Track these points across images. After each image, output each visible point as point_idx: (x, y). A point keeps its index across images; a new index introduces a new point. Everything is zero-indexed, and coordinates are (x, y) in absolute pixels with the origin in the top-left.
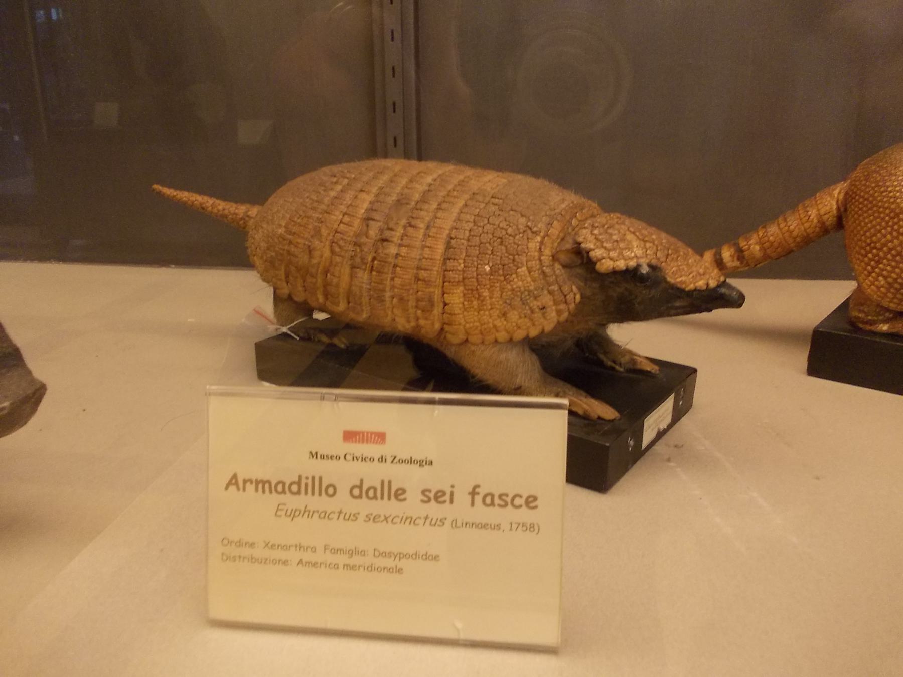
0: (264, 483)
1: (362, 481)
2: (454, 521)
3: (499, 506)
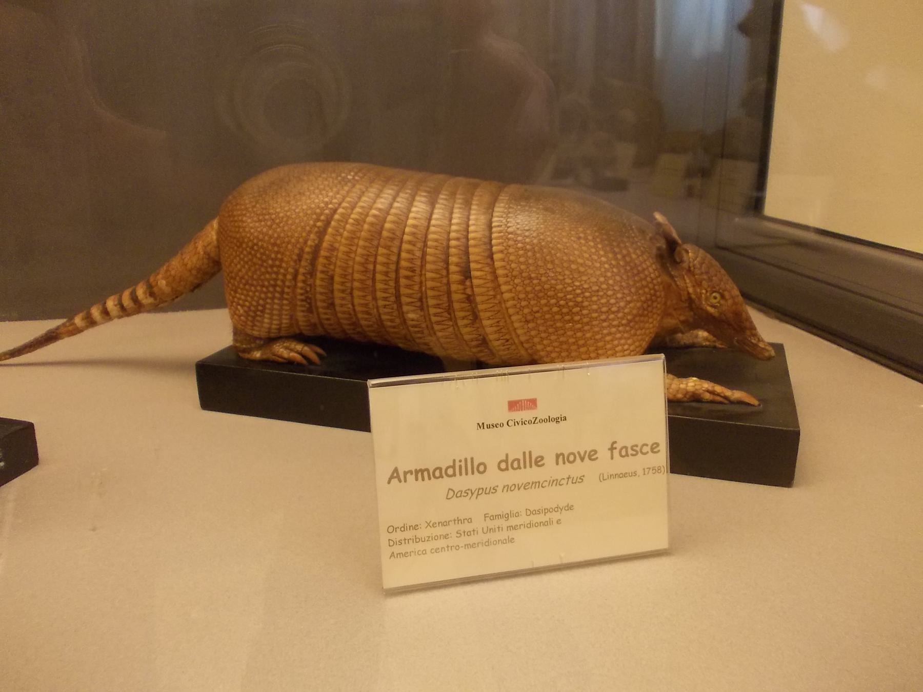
0: (422, 471)
2: (602, 475)
3: (633, 455)
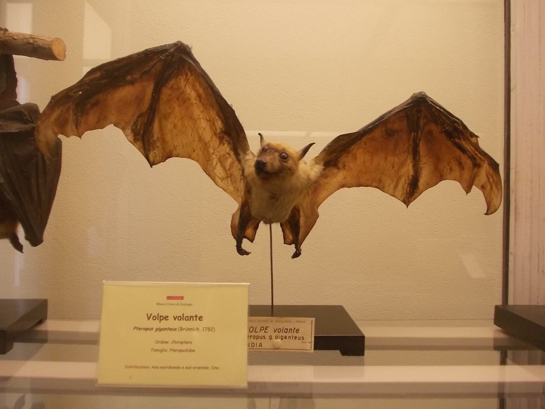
1: (160, 322)
